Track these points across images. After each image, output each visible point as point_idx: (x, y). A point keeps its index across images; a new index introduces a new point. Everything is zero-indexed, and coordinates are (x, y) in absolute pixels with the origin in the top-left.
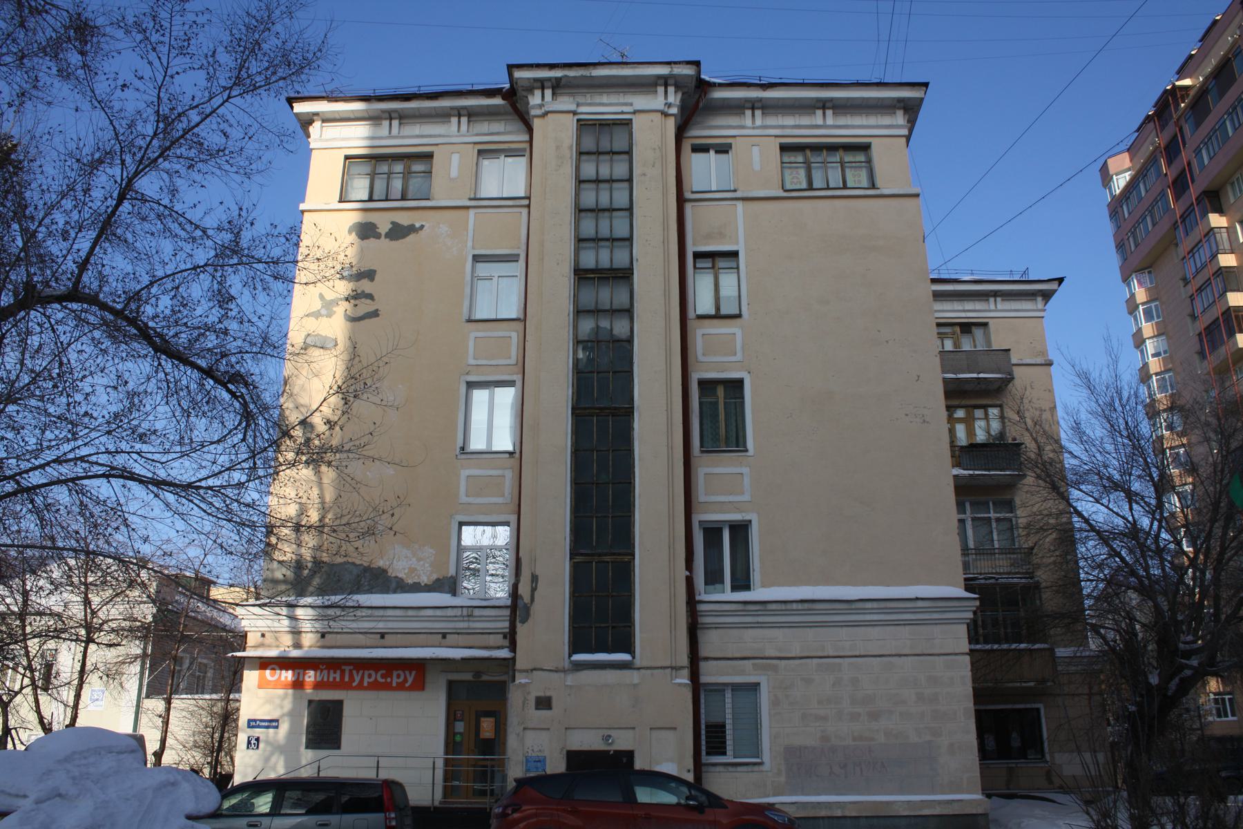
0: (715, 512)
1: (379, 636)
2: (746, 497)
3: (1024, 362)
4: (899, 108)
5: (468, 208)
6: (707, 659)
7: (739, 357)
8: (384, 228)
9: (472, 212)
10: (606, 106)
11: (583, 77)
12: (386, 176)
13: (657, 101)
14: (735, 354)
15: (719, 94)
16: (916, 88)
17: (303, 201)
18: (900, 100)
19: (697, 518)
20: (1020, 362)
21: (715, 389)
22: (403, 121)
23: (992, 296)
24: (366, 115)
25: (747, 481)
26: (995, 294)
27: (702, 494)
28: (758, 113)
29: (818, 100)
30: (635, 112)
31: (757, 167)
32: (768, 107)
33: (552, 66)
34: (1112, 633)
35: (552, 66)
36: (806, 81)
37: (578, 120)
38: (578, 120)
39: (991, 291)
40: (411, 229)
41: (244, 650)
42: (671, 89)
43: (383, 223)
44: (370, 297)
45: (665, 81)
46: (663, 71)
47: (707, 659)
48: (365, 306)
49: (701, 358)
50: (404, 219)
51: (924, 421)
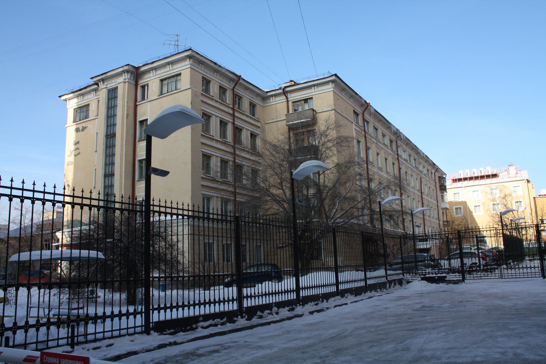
3: (324, 111)
8: (81, 129)
9: (97, 119)
10: (111, 84)
13: (121, 79)
15: (142, 69)
17: (66, 124)
18: (186, 56)
20: (322, 111)
24: (75, 96)
26: (314, 86)
29: (166, 63)
31: (154, 90)
32: (155, 69)
33: (99, 76)
34: (164, 225)
35: (99, 76)
37: (108, 89)
39: (312, 85)
43: (80, 127)
45: (124, 72)
46: (121, 70)
48: (78, 151)
49: (139, 154)
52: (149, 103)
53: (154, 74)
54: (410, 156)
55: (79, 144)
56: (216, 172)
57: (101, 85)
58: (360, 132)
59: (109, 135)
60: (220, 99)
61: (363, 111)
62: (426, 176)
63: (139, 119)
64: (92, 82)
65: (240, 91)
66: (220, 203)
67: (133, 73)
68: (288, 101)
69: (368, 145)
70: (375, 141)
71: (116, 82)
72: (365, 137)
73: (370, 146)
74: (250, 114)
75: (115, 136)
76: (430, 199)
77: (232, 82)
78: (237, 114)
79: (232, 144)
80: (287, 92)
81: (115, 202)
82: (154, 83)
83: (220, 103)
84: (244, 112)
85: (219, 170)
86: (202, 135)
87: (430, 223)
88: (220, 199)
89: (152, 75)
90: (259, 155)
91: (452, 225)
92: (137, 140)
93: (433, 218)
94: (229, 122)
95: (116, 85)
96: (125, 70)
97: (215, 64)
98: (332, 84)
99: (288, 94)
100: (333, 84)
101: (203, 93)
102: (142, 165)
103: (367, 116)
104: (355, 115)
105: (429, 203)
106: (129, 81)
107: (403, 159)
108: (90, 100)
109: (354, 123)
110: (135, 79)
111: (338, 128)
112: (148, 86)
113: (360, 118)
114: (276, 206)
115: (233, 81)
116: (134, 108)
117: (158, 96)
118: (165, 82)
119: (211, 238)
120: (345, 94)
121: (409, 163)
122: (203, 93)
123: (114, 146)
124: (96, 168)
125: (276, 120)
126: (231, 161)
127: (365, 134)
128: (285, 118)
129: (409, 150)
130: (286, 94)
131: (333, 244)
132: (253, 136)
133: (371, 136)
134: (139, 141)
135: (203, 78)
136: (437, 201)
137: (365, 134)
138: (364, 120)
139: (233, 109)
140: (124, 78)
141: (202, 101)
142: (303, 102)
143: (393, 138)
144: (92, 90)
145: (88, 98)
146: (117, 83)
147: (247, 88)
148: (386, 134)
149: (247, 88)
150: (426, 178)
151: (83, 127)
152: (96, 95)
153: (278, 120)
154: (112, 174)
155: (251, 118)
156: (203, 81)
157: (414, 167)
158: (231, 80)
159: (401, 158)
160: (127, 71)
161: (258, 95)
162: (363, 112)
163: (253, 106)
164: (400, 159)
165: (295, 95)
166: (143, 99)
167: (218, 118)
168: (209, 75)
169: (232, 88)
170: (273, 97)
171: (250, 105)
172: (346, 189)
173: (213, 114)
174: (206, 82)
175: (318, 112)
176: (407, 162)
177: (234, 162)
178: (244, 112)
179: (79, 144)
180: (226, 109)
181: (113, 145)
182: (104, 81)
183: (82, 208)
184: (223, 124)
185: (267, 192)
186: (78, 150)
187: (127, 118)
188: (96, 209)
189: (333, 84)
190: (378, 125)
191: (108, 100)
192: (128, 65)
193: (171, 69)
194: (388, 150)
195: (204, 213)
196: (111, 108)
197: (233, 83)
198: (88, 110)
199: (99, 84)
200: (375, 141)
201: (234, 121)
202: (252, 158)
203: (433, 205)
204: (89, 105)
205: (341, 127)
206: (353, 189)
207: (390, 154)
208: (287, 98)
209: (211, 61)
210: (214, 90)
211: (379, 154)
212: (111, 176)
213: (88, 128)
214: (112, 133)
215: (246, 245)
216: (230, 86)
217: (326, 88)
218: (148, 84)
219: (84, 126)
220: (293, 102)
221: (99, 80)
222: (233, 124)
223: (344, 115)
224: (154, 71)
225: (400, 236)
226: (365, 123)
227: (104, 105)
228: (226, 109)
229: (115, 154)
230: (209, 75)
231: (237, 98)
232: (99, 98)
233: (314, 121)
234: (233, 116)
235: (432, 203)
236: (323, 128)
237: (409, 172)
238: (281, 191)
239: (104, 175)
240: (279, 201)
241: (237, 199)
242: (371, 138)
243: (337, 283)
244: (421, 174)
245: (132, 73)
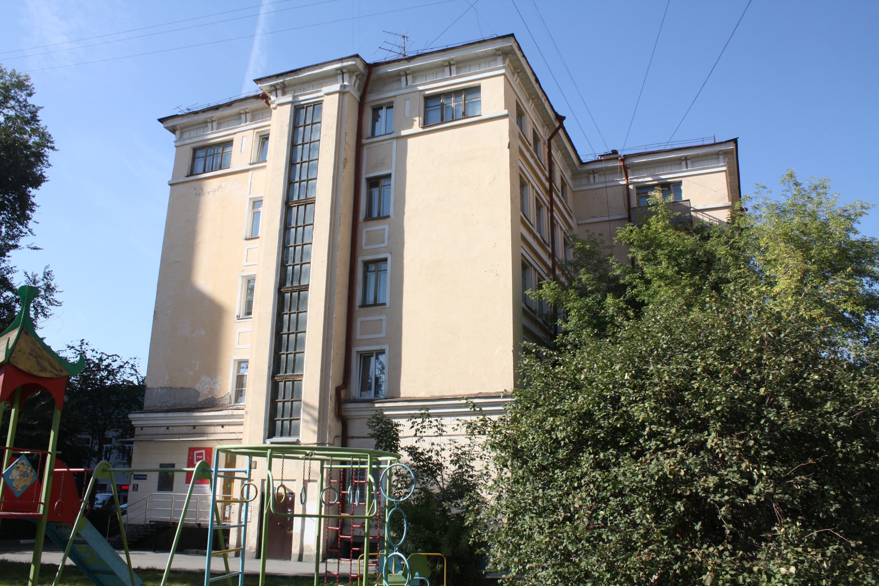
0: (365, 345)
1: (192, 427)
2: (383, 335)
6: (353, 437)
7: (386, 244)
9: (250, 172)
12: (440, 107)
14: (384, 242)
16: (506, 39)
19: (355, 349)
22: (183, 131)
25: (384, 324)
27: (358, 335)
28: (453, 68)
36: (449, 47)
41: (133, 437)
42: (346, 76)
45: (342, 72)
47: (353, 437)
49: (364, 247)
51: (497, 274)
63: (366, 174)
64: (255, 89)
82: (408, 103)
97: (537, 80)
98: (724, 157)
116: (354, 149)
118: (201, 153)
125: (607, 218)
153: (611, 218)
160: (351, 71)
182: (286, 90)
192: (357, 56)
209: (534, 74)
243: (304, 516)
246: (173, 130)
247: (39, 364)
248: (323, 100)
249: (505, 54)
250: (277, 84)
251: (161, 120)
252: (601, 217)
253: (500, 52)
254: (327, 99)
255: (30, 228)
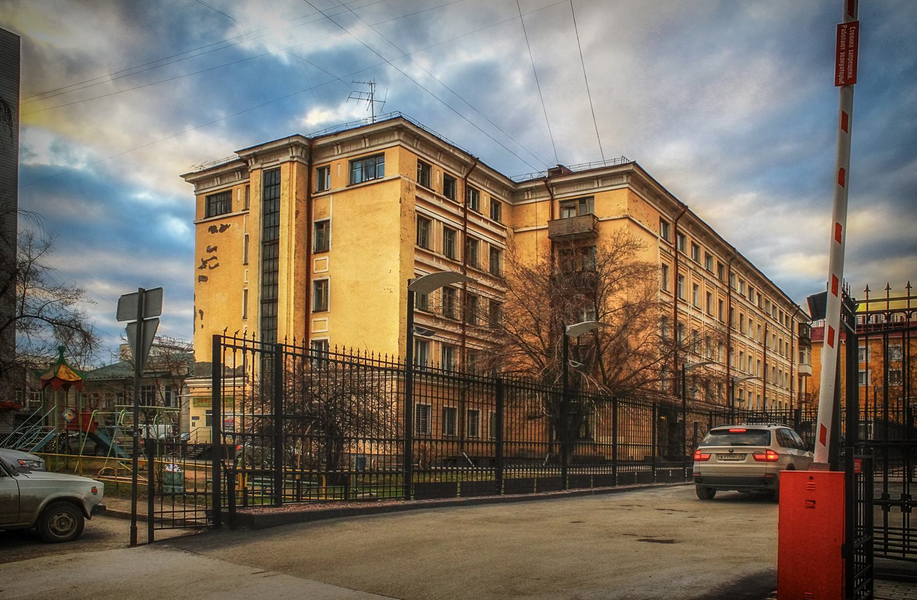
3: (610, 218)
4: (395, 131)
5: (243, 214)
8: (218, 228)
9: (245, 216)
10: (270, 165)
11: (260, 151)
20: (609, 218)
21: (585, 201)
23: (595, 179)
26: (597, 178)
27: (312, 330)
30: (281, 163)
32: (342, 143)
33: (249, 149)
37: (264, 171)
38: (264, 171)
40: (227, 226)
44: (216, 258)
45: (290, 146)
46: (286, 142)
50: (224, 223)
52: (331, 196)
53: (340, 152)
54: (751, 289)
55: (216, 251)
56: (438, 308)
57: (253, 165)
58: (667, 252)
59: (267, 242)
60: (444, 194)
61: (675, 218)
62: (776, 322)
64: (237, 157)
65: (474, 182)
66: (440, 349)
67: (305, 147)
68: (552, 200)
69: (679, 272)
70: (692, 266)
71: (278, 160)
72: (676, 259)
73: (683, 274)
74: (491, 217)
75: (278, 243)
76: (779, 359)
77: (463, 167)
78: (470, 218)
79: (462, 264)
80: (553, 185)
81: (427, 368)
83: (444, 200)
84: (482, 214)
85: (441, 304)
86: (416, 249)
87: (775, 395)
88: (440, 345)
89: (336, 153)
90: (502, 281)
91: (813, 400)
92: (312, 252)
93: (781, 387)
94: (458, 229)
95: (277, 165)
96: (293, 143)
99: (554, 188)
100: (630, 178)
101: (418, 185)
102: (320, 288)
103: (682, 227)
104: (662, 224)
105: (776, 364)
106: (299, 160)
107: (738, 294)
108: (233, 184)
109: (660, 237)
110: (308, 157)
111: (634, 251)
112: (329, 171)
113: (671, 228)
114: (529, 362)
115: (465, 166)
117: (347, 186)
119: (429, 399)
120: (647, 192)
121: (747, 301)
122: (418, 185)
123: (276, 258)
124: (246, 288)
125: (535, 228)
126: (459, 290)
127: (677, 255)
128: (547, 226)
129: (748, 282)
130: (551, 189)
131: (612, 417)
132: (495, 252)
133: (687, 258)
134: (315, 253)
135: (419, 161)
136: (792, 361)
137: (677, 255)
138: (677, 232)
139: (464, 210)
140: (291, 155)
141: (417, 198)
142: (577, 202)
143: (724, 261)
144: (237, 170)
145: (230, 181)
146: (278, 162)
147: (486, 177)
148: (712, 255)
149: (486, 177)
150: (776, 325)
151: (221, 225)
152: (242, 178)
153: (538, 228)
154: (273, 300)
155: (491, 223)
156: (418, 166)
157: (756, 307)
158: (462, 164)
159: (735, 293)
161: (503, 187)
162: (677, 220)
163: (495, 205)
164: (732, 294)
165: (566, 191)
166: (321, 188)
167: (441, 223)
168: (428, 158)
169: (463, 176)
170: (529, 192)
171: (491, 202)
172: (637, 339)
173: (433, 218)
174: (424, 171)
175: (602, 219)
176: (745, 300)
177: (464, 290)
178: (482, 214)
179: (216, 251)
180: (454, 210)
181: (275, 257)
183: (235, 351)
184: (449, 232)
185: (515, 341)
186: (214, 260)
187: (296, 217)
188: (291, 357)
189: (630, 178)
190: (698, 241)
191: (265, 187)
193: (367, 145)
194: (712, 281)
195: (443, 370)
196: (270, 200)
197: (466, 169)
198: (229, 201)
199: (249, 161)
200: (692, 266)
201: (465, 228)
202: (497, 287)
203: (783, 368)
204: (230, 192)
205: (638, 249)
206: (650, 341)
207: (717, 286)
208: (552, 195)
210: (437, 179)
211: (698, 286)
212: (273, 303)
213: (230, 227)
214: (272, 238)
215: (478, 412)
216: (461, 173)
217: (616, 183)
218: (330, 165)
219: (225, 224)
220: (561, 202)
221: (249, 156)
222: (464, 232)
223: (645, 227)
224: (339, 147)
225: (711, 412)
226: (679, 237)
227: (259, 196)
228: (454, 210)
229: (278, 271)
230: (428, 158)
231: (472, 194)
232: (249, 182)
233: (593, 234)
234: (464, 220)
235: (783, 364)
236: (609, 250)
237: (748, 316)
238: (537, 338)
239: (261, 301)
240: (535, 354)
241: (467, 345)
242: (685, 261)
244: (766, 318)
245: (303, 148)
246: (192, 182)
247: (69, 376)
248: (280, 167)
249: (400, 129)
250: (251, 154)
251: (181, 176)
252: (295, 251)
253: (395, 129)
254: (283, 166)
255: (539, 169)
